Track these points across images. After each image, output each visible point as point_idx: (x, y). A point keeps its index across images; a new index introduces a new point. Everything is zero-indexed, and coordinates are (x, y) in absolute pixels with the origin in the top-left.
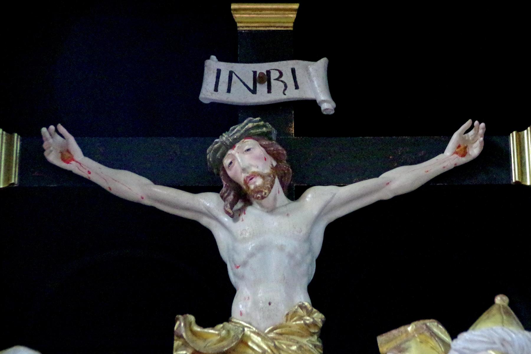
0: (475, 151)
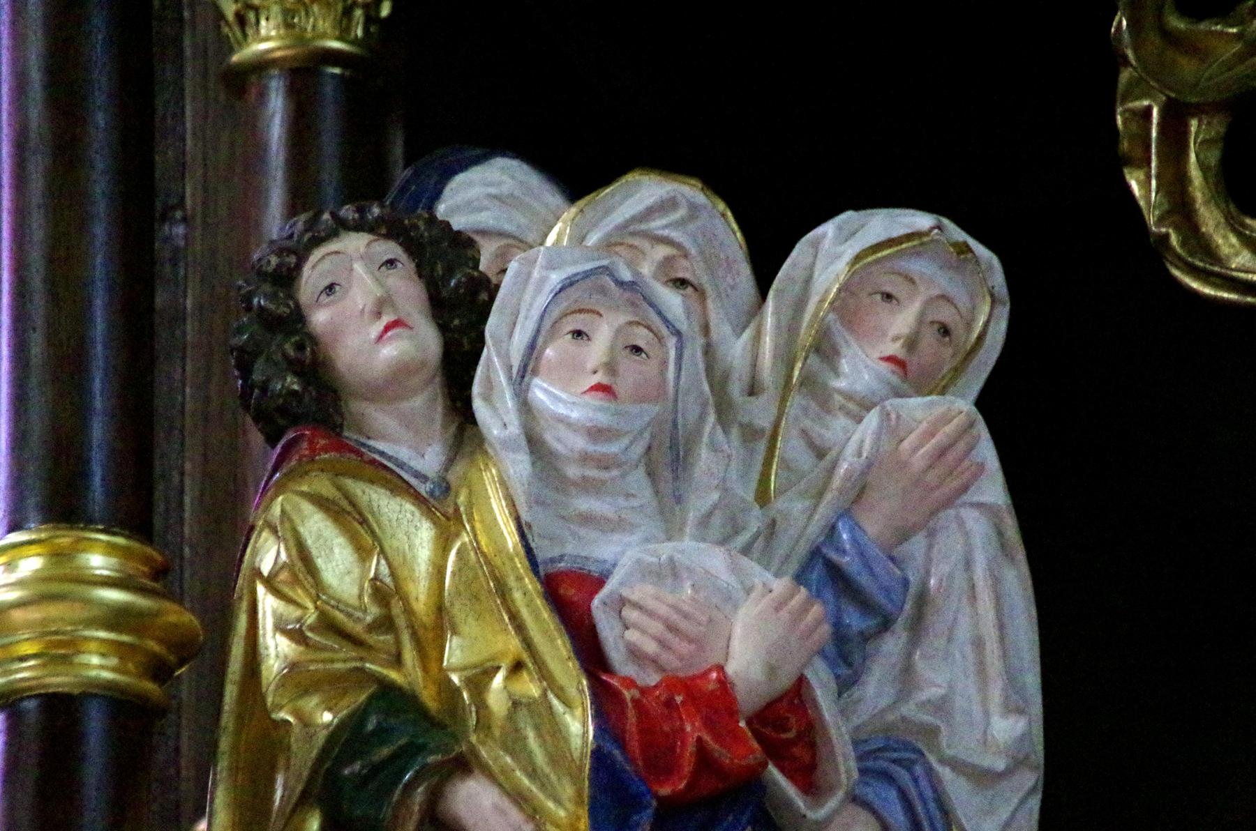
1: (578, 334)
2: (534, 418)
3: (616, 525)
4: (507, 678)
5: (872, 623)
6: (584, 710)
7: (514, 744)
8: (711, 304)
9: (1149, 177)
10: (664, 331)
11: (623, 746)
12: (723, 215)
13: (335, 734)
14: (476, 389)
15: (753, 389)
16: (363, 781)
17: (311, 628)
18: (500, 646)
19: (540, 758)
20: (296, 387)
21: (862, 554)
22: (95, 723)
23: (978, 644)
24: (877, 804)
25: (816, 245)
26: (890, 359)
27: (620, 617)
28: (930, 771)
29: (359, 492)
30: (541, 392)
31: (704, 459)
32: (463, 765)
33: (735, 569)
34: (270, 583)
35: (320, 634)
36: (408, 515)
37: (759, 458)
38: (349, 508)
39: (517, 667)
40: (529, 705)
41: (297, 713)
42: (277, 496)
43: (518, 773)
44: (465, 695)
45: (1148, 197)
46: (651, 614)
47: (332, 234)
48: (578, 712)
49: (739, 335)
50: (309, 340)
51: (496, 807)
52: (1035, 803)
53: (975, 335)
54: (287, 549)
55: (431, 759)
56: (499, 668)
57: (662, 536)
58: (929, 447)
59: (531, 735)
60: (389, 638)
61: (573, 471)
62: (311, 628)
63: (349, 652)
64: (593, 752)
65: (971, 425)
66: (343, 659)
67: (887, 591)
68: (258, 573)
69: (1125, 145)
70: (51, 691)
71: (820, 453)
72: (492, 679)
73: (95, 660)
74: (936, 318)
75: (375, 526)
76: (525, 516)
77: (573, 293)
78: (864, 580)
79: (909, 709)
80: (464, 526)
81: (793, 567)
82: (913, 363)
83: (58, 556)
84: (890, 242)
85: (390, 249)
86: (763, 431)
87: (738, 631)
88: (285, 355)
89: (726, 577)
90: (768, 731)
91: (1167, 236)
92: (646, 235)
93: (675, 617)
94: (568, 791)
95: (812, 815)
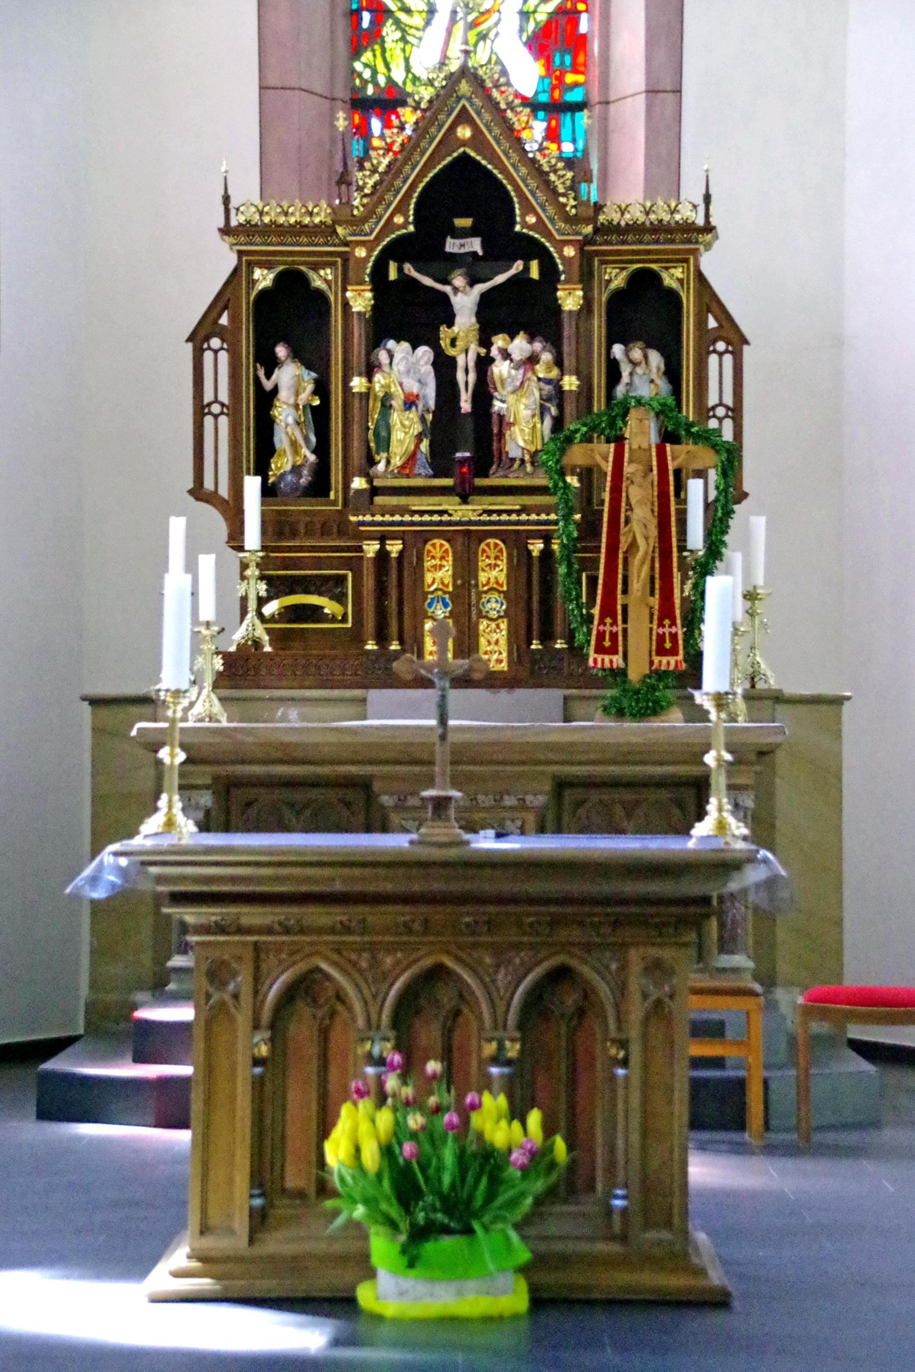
0: (521, 268)
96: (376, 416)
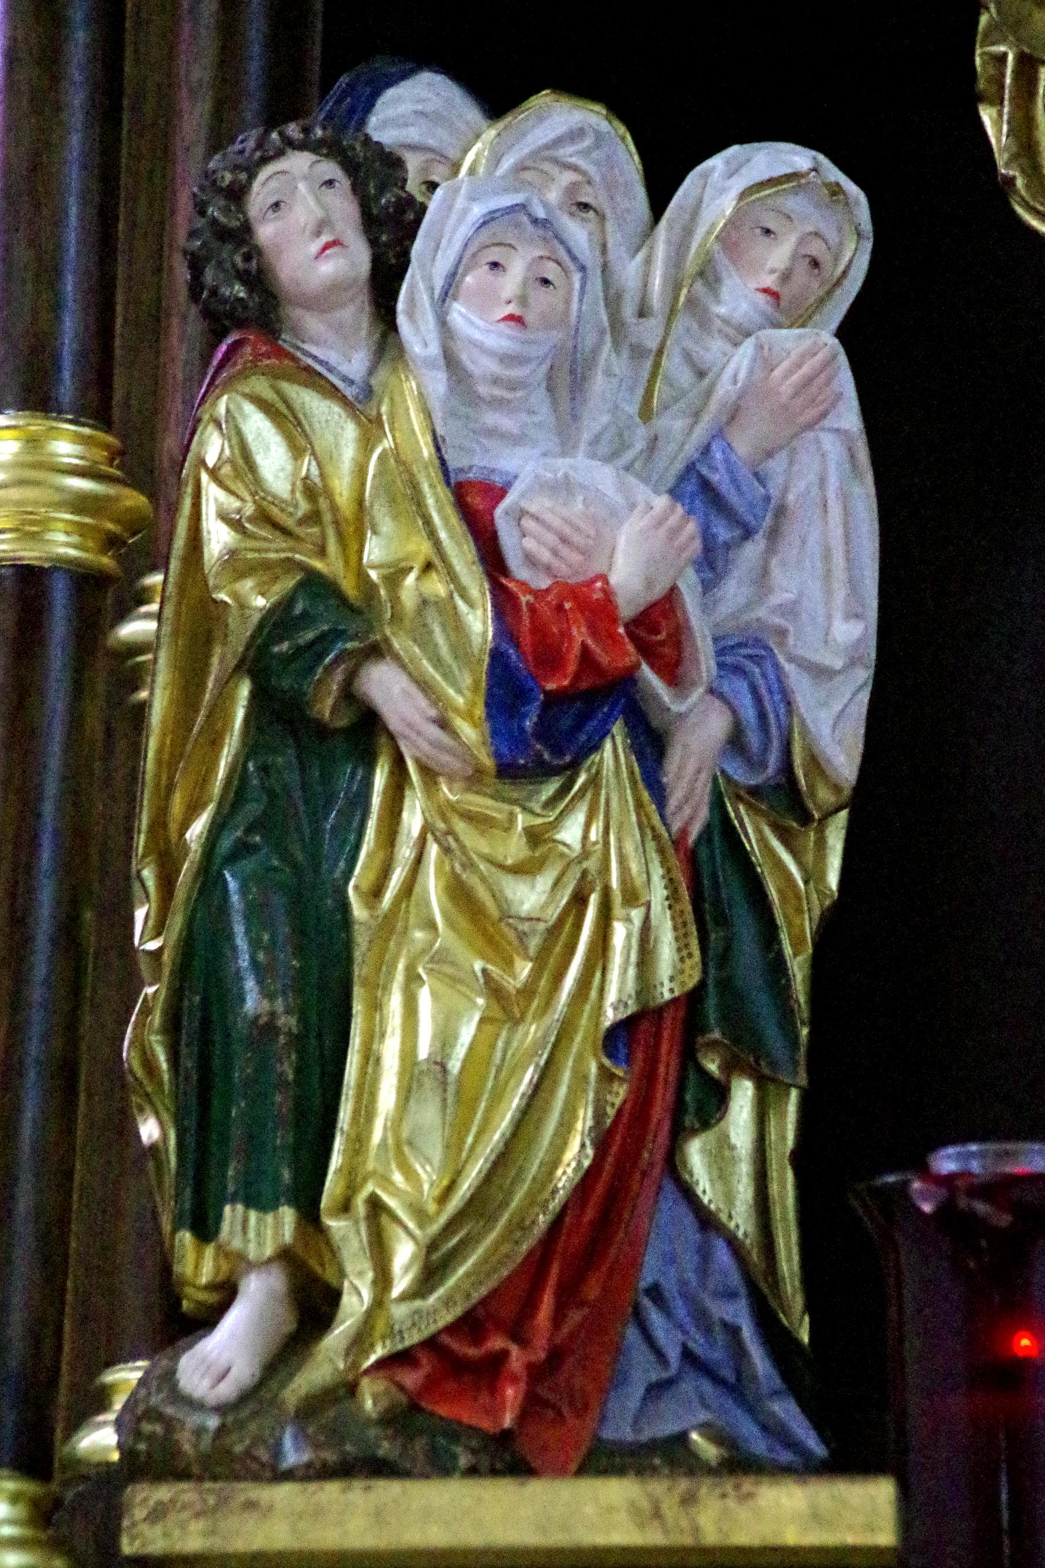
1: (495, 265)
2: (452, 338)
3: (517, 440)
4: (418, 579)
5: (738, 532)
6: (485, 610)
7: (424, 640)
8: (610, 226)
9: (1000, 114)
10: (572, 267)
11: (517, 646)
12: (623, 139)
13: (269, 614)
14: (401, 305)
15: (643, 312)
16: (287, 659)
17: (250, 520)
18: (412, 547)
19: (444, 651)
20: (242, 295)
21: (730, 471)
22: (60, 594)
23: (827, 556)
24: (730, 696)
25: (706, 176)
26: (766, 291)
27: (519, 524)
28: (777, 666)
29: (294, 395)
30: (458, 313)
31: (599, 384)
32: (377, 651)
33: (622, 487)
34: (214, 474)
35: (256, 524)
36: (336, 417)
37: (646, 375)
38: (285, 411)
39: (428, 567)
40: (436, 603)
41: (235, 596)
42: (222, 395)
43: (424, 662)
44: (382, 592)
45: (999, 140)
46: (548, 527)
47: (280, 154)
48: (479, 612)
49: (633, 257)
50: (255, 252)
51: (404, 691)
52: (865, 697)
53: (841, 268)
54: (231, 446)
55: (349, 645)
56: (411, 568)
57: (558, 449)
58: (796, 378)
59: (437, 630)
60: (315, 530)
61: (483, 390)
62: (250, 520)
63: (281, 543)
64: (491, 650)
65: (834, 357)
66: (276, 549)
67: (751, 505)
68: (203, 462)
69: (982, 84)
70: (25, 563)
71: (701, 374)
72: (404, 579)
73: (62, 538)
74: (809, 253)
75: (307, 427)
76: (440, 431)
77: (493, 227)
78: (733, 498)
79: (761, 612)
80: (385, 433)
81: (670, 480)
82: (786, 293)
83: (33, 442)
84: (771, 182)
85: (330, 169)
86: (651, 351)
87: (622, 542)
88: (234, 265)
89: (618, 499)
90: (642, 633)
91: (1014, 178)
92: (556, 161)
93: (567, 530)
94: (467, 680)
95: (676, 708)
96: (198, 829)
